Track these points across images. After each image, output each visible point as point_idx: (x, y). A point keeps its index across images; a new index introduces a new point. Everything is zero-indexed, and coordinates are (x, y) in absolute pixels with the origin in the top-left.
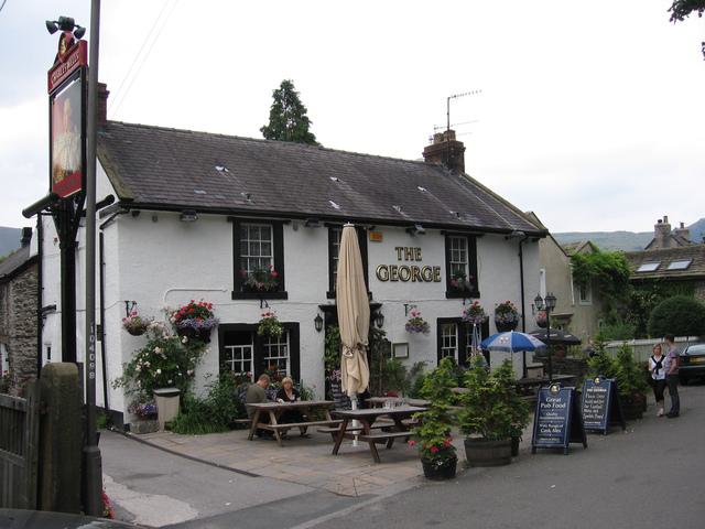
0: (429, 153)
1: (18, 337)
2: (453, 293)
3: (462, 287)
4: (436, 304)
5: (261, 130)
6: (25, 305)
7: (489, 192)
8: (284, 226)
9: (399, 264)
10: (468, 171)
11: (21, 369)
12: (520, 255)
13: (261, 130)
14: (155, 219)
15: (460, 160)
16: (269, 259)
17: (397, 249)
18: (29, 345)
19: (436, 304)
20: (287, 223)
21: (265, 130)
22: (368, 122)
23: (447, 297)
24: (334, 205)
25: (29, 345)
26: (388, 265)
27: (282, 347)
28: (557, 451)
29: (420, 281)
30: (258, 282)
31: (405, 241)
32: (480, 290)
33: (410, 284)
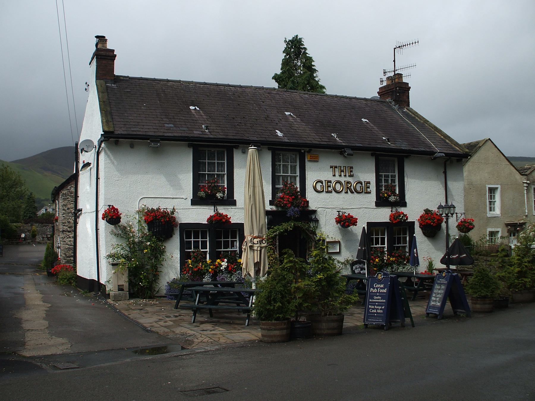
0: (383, 92)
1: (63, 231)
2: (381, 202)
3: (390, 196)
4: (367, 211)
5: (273, 78)
6: (68, 209)
7: (426, 121)
8: (234, 150)
9: (333, 179)
10: (413, 105)
11: (65, 254)
12: (445, 173)
13: (273, 78)
14: (132, 146)
15: (248, 90)
16: (395, 185)
17: (331, 167)
18: (70, 237)
19: (367, 211)
20: (237, 147)
21: (276, 78)
22: (349, 74)
23: (376, 206)
24: (279, 134)
25: (70, 237)
26: (323, 180)
27: (233, 242)
28: (380, 328)
29: (352, 192)
30: (210, 190)
31: (338, 162)
32: (407, 201)
33: (324, 194)
